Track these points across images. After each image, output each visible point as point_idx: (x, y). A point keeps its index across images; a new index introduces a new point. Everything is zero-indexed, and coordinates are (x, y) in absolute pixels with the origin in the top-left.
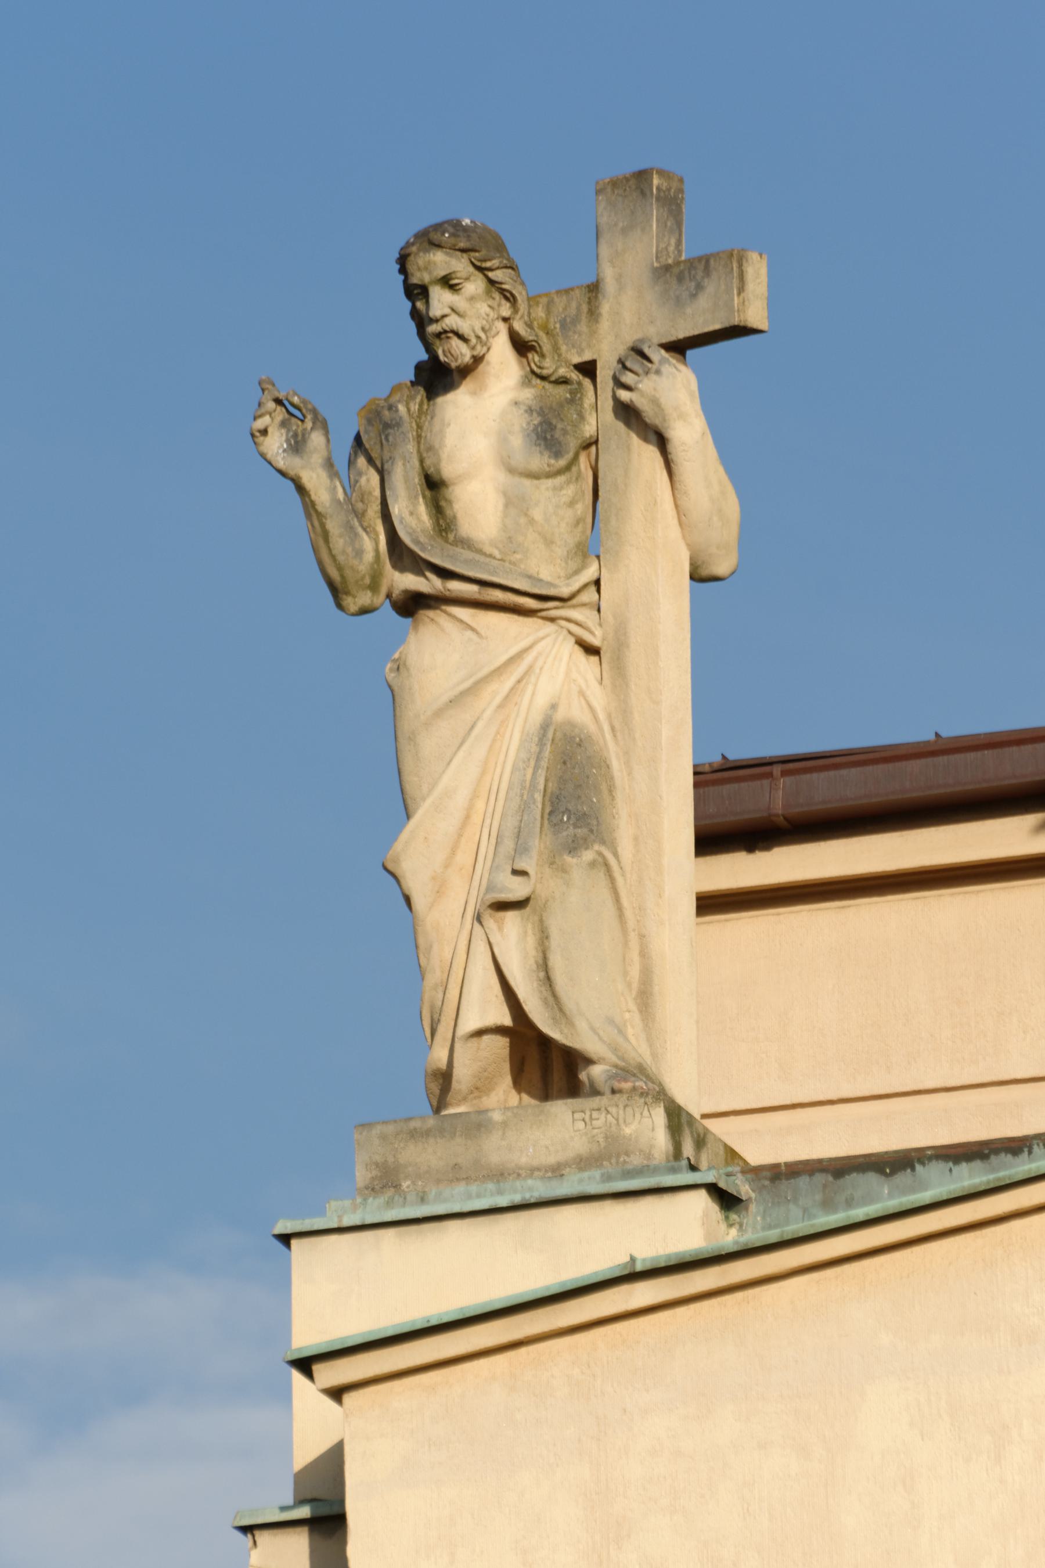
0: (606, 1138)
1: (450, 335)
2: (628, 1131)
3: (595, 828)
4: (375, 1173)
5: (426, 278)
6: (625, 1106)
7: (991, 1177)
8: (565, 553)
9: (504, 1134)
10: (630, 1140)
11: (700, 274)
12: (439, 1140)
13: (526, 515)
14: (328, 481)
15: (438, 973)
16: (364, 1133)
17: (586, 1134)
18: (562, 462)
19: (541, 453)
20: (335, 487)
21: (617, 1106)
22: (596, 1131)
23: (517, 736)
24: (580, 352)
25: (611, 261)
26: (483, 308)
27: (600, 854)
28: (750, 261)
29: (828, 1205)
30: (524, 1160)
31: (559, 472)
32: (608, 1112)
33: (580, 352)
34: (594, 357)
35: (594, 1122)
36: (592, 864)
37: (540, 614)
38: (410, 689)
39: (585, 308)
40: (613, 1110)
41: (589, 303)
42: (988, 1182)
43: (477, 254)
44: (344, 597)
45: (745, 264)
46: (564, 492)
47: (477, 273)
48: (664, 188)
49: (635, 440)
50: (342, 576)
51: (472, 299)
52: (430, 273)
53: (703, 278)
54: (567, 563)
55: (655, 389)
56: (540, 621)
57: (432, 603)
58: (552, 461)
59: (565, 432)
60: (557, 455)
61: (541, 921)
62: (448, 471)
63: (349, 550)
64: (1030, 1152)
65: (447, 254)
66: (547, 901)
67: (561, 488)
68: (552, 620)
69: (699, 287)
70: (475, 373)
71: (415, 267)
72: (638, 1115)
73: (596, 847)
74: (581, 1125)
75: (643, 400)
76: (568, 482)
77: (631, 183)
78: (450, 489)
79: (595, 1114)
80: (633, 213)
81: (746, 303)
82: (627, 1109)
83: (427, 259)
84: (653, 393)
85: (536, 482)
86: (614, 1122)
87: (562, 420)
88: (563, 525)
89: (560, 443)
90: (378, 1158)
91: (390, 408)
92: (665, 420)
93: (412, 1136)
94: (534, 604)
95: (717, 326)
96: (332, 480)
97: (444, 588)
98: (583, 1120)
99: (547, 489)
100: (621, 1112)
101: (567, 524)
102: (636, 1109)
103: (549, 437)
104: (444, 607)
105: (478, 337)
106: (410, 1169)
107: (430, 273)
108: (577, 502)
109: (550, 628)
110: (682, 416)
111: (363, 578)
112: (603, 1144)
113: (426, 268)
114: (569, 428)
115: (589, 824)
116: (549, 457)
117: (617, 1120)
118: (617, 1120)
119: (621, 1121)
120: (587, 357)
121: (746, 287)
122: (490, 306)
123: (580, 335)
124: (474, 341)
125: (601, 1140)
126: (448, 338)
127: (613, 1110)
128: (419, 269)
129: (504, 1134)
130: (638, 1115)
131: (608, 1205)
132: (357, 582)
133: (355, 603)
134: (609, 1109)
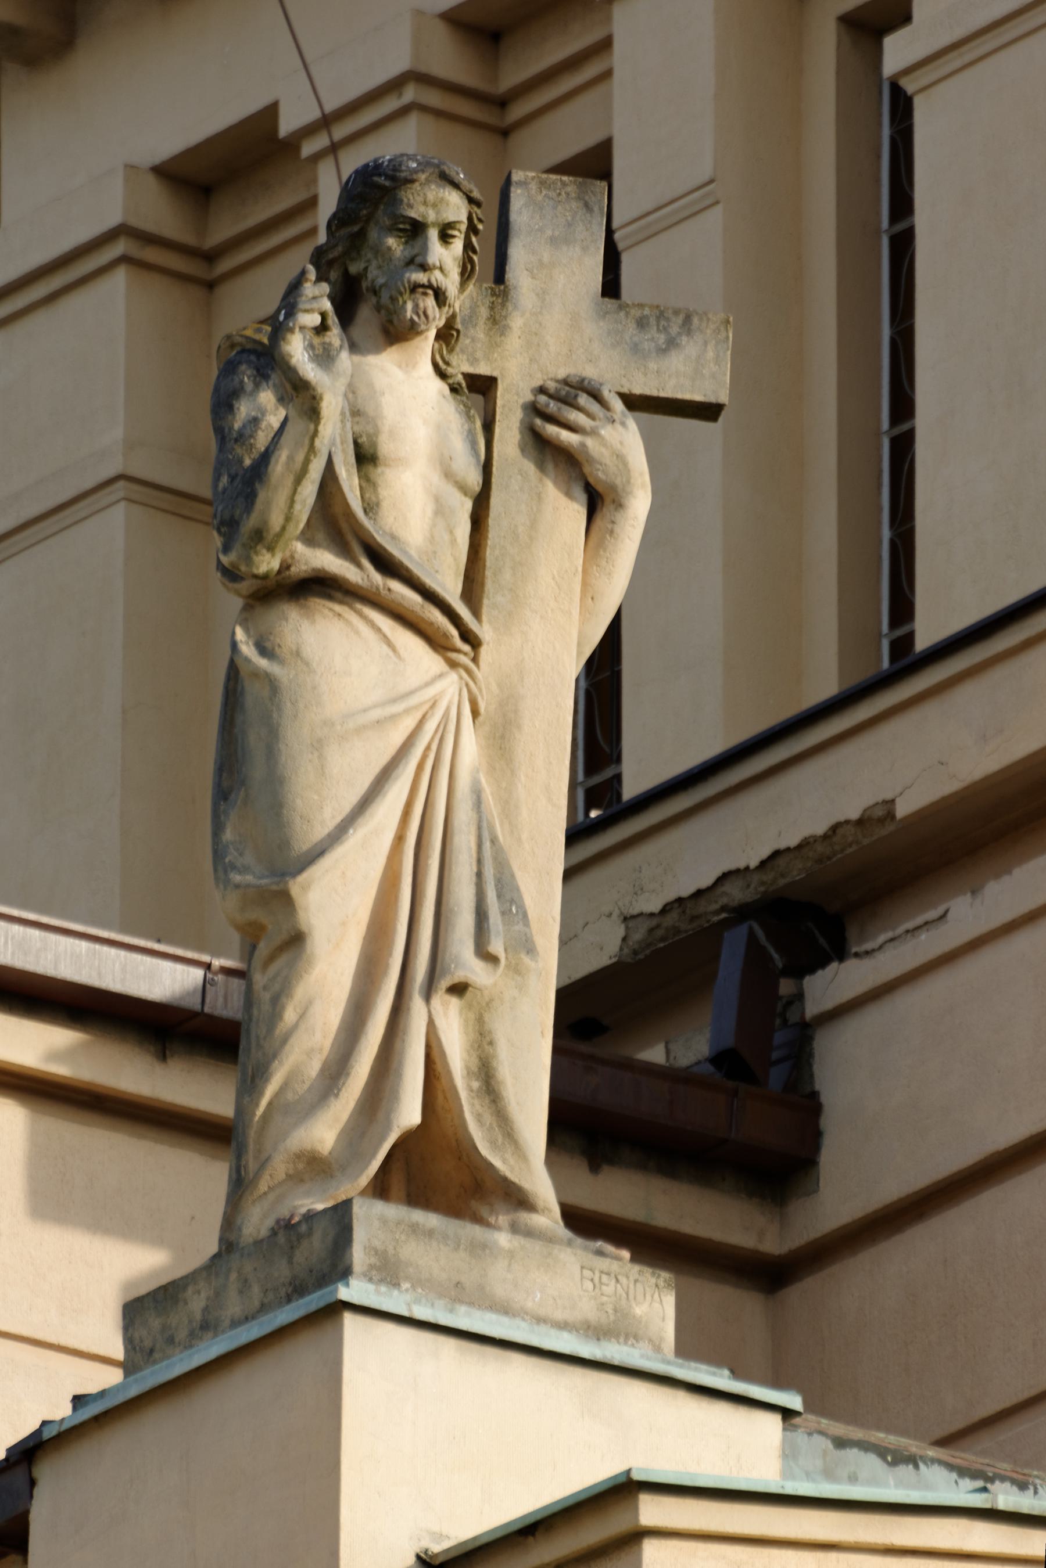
0: (615, 1311)
1: (430, 292)
2: (639, 1310)
4: (373, 1260)
5: (431, 216)
6: (636, 1281)
9: (510, 1265)
10: (640, 1322)
11: (674, 330)
12: (442, 1246)
15: (318, 1035)
16: (364, 1209)
17: (595, 1299)
21: (628, 1277)
22: (605, 1299)
23: (490, 798)
24: (474, 361)
25: (530, 271)
29: (829, 1474)
30: (529, 1304)
32: (617, 1281)
33: (474, 361)
34: (495, 374)
35: (604, 1288)
38: (314, 688)
39: (484, 312)
40: (623, 1280)
41: (492, 308)
44: (264, 551)
49: (551, 491)
50: (284, 528)
52: (438, 213)
53: (679, 334)
55: (621, 443)
57: (339, 595)
61: (480, 1020)
62: (386, 447)
64: (1036, 1492)
66: (491, 1000)
69: (672, 344)
70: (406, 345)
71: (420, 199)
72: (648, 1297)
74: (589, 1285)
75: (603, 450)
77: (569, 189)
78: (379, 470)
79: (605, 1278)
80: (569, 225)
82: (639, 1285)
83: (440, 195)
84: (619, 446)
86: (624, 1295)
90: (377, 1243)
91: (670, 376)
92: (628, 482)
93: (414, 1231)
95: (698, 397)
97: (384, 585)
98: (592, 1280)
100: (632, 1286)
102: (647, 1289)
104: (359, 606)
106: (411, 1270)
107: (438, 213)
112: (612, 1318)
113: (434, 206)
117: (627, 1294)
118: (627, 1294)
119: (631, 1297)
120: (483, 369)
123: (473, 340)
125: (611, 1311)
126: (425, 294)
127: (623, 1280)
128: (425, 203)
129: (510, 1265)
130: (648, 1297)
131: (682, 1397)
133: (269, 563)
134: (620, 1277)
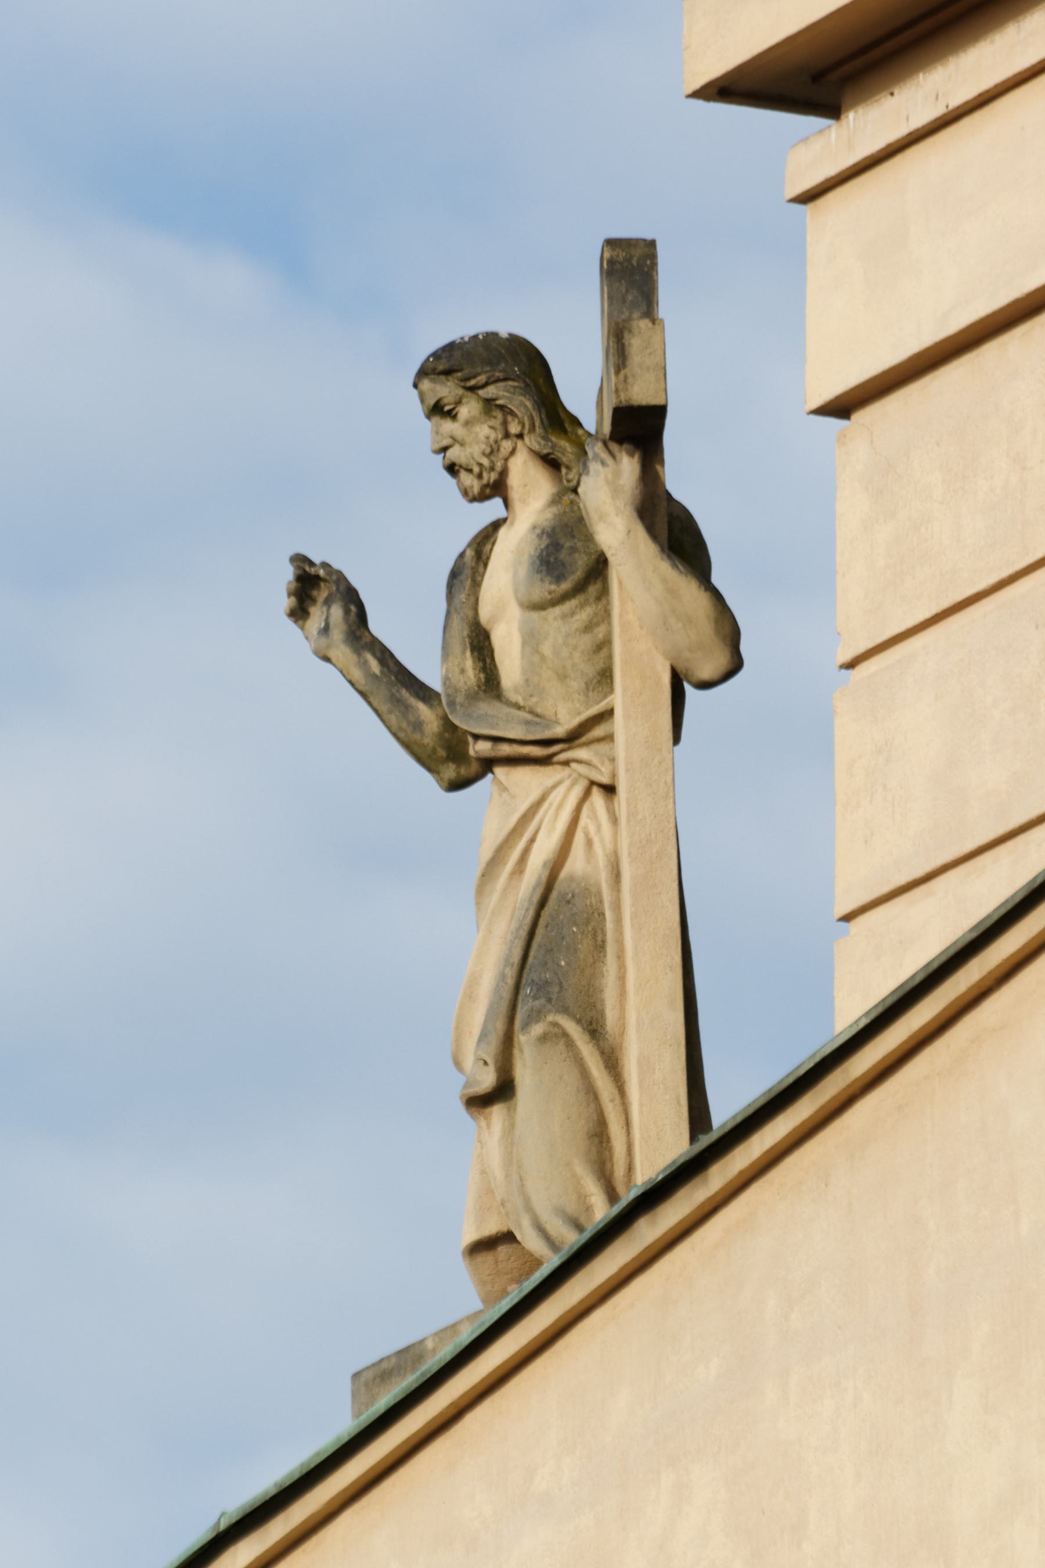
3: (554, 997)
7: (418, 1373)
8: (583, 685)
13: (538, 652)
14: (355, 657)
18: (566, 586)
19: (542, 580)
20: (366, 661)
26: (484, 431)
27: (556, 1025)
28: (636, 331)
31: (564, 597)
36: (544, 1038)
37: (556, 759)
42: (417, 1379)
43: (459, 374)
45: (626, 335)
46: (577, 617)
47: (469, 394)
48: (621, 258)
51: (467, 423)
54: (587, 696)
56: (559, 767)
58: (553, 587)
59: (573, 550)
60: (559, 579)
63: (404, 725)
65: (433, 381)
67: (573, 614)
68: (566, 763)
73: (550, 1018)
76: (582, 606)
81: (630, 380)
85: (543, 613)
87: (573, 537)
88: (577, 655)
89: (563, 565)
94: (545, 751)
96: (359, 655)
99: (555, 619)
101: (582, 652)
103: (552, 560)
105: (480, 465)
108: (597, 624)
109: (565, 772)
110: (602, 517)
111: (434, 751)
114: (579, 545)
115: (548, 992)
116: (550, 583)
121: (629, 363)
122: (491, 427)
124: (476, 469)
132: (429, 756)
